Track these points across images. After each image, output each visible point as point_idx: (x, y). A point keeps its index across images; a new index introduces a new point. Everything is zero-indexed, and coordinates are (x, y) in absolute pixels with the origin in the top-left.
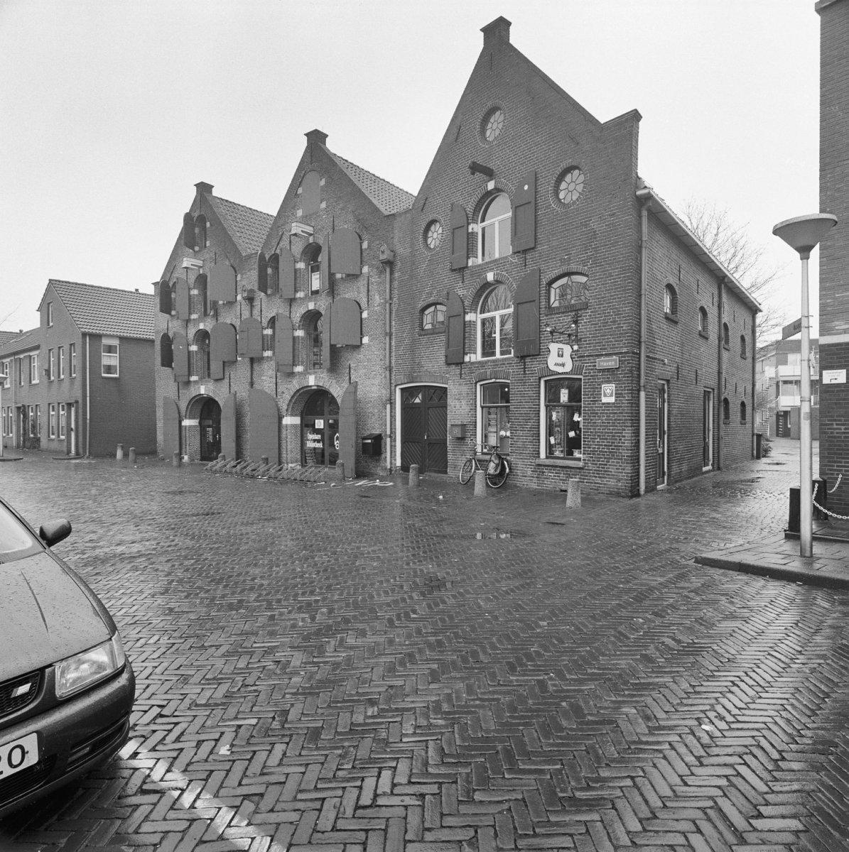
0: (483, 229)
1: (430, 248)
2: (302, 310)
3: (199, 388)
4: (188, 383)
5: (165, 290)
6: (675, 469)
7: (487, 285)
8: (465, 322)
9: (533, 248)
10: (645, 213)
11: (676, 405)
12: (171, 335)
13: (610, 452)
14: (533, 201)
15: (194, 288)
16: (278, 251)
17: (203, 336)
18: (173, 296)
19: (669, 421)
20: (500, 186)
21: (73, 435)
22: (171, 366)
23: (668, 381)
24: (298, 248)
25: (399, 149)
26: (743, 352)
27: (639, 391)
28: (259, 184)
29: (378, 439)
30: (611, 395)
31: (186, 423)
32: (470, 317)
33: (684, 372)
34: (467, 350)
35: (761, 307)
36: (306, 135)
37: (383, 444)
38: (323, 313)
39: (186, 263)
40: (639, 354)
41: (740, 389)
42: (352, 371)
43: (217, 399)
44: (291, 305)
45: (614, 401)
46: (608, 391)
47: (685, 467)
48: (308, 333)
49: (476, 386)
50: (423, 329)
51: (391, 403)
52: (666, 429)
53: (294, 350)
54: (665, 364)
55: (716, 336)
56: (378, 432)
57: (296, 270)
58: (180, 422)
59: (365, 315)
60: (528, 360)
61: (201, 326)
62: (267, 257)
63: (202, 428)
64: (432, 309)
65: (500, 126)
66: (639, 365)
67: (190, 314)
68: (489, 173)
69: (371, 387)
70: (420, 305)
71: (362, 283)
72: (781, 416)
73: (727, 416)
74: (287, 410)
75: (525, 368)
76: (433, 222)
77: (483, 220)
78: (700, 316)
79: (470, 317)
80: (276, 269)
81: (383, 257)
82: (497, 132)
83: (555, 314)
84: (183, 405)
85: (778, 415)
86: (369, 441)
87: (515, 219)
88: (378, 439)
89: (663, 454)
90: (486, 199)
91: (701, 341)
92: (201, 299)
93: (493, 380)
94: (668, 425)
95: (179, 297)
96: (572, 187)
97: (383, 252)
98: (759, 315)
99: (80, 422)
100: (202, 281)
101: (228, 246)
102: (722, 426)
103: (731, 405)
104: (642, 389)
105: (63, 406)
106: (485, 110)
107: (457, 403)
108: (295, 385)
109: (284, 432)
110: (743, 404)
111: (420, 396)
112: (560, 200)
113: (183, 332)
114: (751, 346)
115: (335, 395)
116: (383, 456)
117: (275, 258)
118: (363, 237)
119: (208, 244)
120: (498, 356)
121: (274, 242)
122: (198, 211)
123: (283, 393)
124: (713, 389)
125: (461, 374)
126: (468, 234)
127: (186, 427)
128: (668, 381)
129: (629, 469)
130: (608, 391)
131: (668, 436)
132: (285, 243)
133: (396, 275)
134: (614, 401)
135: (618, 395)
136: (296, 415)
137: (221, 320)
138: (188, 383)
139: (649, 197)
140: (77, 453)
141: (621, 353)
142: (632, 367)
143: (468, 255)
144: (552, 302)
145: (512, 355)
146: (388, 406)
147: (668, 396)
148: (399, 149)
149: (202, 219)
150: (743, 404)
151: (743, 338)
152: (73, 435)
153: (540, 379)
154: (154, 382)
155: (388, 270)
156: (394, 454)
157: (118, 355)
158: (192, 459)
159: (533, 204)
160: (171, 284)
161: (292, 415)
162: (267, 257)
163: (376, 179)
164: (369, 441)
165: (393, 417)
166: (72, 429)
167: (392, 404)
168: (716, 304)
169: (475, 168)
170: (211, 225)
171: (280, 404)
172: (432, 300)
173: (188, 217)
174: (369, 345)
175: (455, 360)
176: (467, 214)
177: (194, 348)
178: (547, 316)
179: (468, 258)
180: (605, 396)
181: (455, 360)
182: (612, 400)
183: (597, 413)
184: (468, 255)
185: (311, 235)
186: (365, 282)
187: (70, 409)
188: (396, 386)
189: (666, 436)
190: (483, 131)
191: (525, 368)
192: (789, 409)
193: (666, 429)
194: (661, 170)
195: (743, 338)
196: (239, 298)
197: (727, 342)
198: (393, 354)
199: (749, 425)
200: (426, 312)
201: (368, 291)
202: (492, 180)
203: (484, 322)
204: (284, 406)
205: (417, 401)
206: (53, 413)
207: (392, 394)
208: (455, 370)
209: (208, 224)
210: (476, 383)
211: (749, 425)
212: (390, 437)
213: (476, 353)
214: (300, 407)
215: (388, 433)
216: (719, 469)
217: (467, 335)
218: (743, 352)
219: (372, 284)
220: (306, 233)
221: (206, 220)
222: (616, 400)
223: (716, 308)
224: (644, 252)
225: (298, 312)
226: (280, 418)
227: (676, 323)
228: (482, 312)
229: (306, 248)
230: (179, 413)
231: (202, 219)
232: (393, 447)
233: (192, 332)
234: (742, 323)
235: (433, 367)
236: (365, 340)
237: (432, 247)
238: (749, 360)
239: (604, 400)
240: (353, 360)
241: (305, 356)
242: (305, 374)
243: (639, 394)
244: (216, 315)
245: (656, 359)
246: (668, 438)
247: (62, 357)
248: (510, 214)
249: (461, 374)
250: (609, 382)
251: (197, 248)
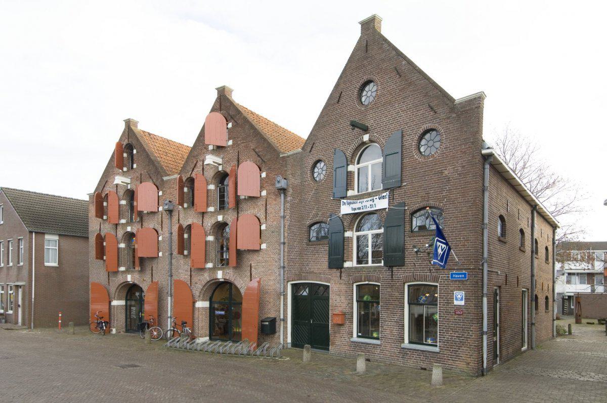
0: (359, 169)
1: (316, 180)
2: (213, 221)
3: (127, 276)
4: (116, 272)
5: (100, 199)
6: (504, 353)
7: (364, 143)
8: (344, 237)
9: (400, 187)
10: (487, 166)
11: (504, 303)
12: (103, 234)
13: (461, 342)
14: (400, 150)
15: (123, 199)
16: (193, 175)
17: (130, 236)
18: (105, 204)
19: (500, 317)
20: (373, 139)
21: (20, 310)
22: (102, 258)
23: (500, 287)
24: (210, 174)
25: (293, 105)
26: (547, 259)
27: (482, 297)
28: (178, 122)
29: (273, 321)
30: (462, 300)
31: (115, 303)
32: (348, 234)
33: (509, 279)
34: (345, 259)
35: (559, 224)
36: (217, 89)
37: (277, 326)
38: (230, 224)
39: (119, 180)
40: (483, 270)
41: (545, 288)
42: (253, 269)
43: (141, 286)
44: (203, 217)
45: (463, 304)
46: (459, 296)
47: (510, 350)
48: (216, 238)
49: (353, 286)
50: (310, 241)
51: (284, 295)
52: (498, 322)
53: (206, 251)
54: (498, 275)
55: (530, 249)
56: (272, 315)
57: (208, 191)
58: (110, 302)
59: (263, 227)
60: (395, 269)
61: (129, 229)
62: (184, 179)
63: (127, 308)
64: (316, 226)
65: (374, 94)
66: (483, 277)
67: (119, 219)
68: (366, 130)
69: (268, 280)
70: (308, 223)
71: (261, 203)
72: (566, 299)
73: (537, 308)
74: (199, 296)
75: (392, 275)
76: (319, 161)
77: (358, 163)
78: (499, 222)
79: (348, 234)
80: (192, 189)
81: (278, 185)
82: (371, 99)
83: (417, 236)
84: (113, 289)
85: (563, 299)
86: (267, 323)
87: (384, 165)
88: (273, 321)
89: (496, 341)
90: (361, 148)
91: (521, 253)
92: (128, 208)
93: (367, 282)
94: (500, 319)
95: (111, 206)
96: (369, 94)
97: (279, 182)
98: (558, 230)
99: (27, 302)
100: (131, 195)
101: (154, 171)
102: (534, 316)
103: (539, 300)
104: (485, 295)
105: (11, 287)
106: (362, 82)
107: (338, 298)
108: (206, 277)
109: (196, 313)
110: (547, 298)
111: (307, 290)
112: (421, 152)
113: (113, 233)
114: (552, 254)
115: (239, 286)
116: (277, 334)
117: (191, 181)
118: (263, 169)
119: (135, 166)
120: (370, 264)
121: (189, 168)
122: (126, 141)
123: (196, 283)
124: (528, 289)
125: (341, 276)
126: (347, 172)
127: (114, 306)
128: (500, 287)
129: (475, 354)
130: (459, 296)
131: (500, 327)
132: (198, 169)
133: (289, 199)
134: (463, 304)
135: (467, 300)
136: (206, 300)
137: (145, 224)
138: (116, 272)
139: (491, 155)
140: (24, 324)
141: (470, 269)
142: (478, 280)
143: (347, 188)
144: (414, 228)
145: (382, 264)
146: (282, 297)
147: (500, 298)
148: (293, 105)
149: (130, 147)
150: (547, 298)
151: (547, 248)
152: (20, 310)
153: (404, 284)
154: (88, 270)
155: (282, 195)
156: (285, 334)
157: (57, 248)
158: (118, 332)
159: (400, 153)
160: (103, 195)
161: (203, 300)
162: (184, 179)
163: (267, 123)
164: (267, 323)
165: (285, 305)
166: (19, 306)
167: (285, 296)
168: (530, 225)
169: (354, 125)
170: (137, 152)
171: (194, 292)
172: (317, 219)
173: (119, 145)
174: (266, 250)
175: (336, 262)
176: (347, 158)
177: (122, 245)
178: (410, 237)
179: (347, 190)
180: (457, 299)
181: (336, 262)
182: (462, 303)
183: (450, 312)
184: (347, 188)
185: (220, 164)
186: (264, 203)
187: (18, 290)
188: (288, 282)
189: (498, 328)
190: (360, 96)
191: (392, 275)
192: (572, 294)
193: (498, 322)
194: (494, 134)
195: (547, 248)
196: (161, 209)
197: (537, 253)
198: (286, 257)
199: (550, 314)
200: (313, 228)
201: (266, 209)
202: (366, 134)
203: (358, 238)
204: (197, 293)
205: (305, 294)
206: (12, 292)
207: (285, 288)
208: (336, 273)
209: (135, 151)
210: (353, 283)
211: (550, 314)
212: (283, 320)
213: (352, 261)
214: (209, 295)
215: (282, 317)
216: (532, 348)
217: (345, 247)
218: (547, 259)
219: (270, 204)
220: (216, 163)
221: (131, 149)
222: (465, 303)
223: (530, 229)
224: (487, 194)
225: (209, 222)
226: (194, 303)
227: (505, 243)
228: (358, 230)
229: (215, 174)
230: (109, 295)
231: (130, 147)
232: (285, 328)
233: (120, 233)
234: (546, 237)
235: (317, 269)
236: (264, 246)
237: (317, 179)
238: (551, 264)
239: (456, 303)
240: (253, 260)
241: (214, 256)
242: (215, 269)
243: (482, 299)
244: (141, 221)
245: (492, 271)
246: (500, 330)
247: (11, 248)
248: (381, 160)
249: (341, 276)
250: (459, 289)
251: (125, 169)
